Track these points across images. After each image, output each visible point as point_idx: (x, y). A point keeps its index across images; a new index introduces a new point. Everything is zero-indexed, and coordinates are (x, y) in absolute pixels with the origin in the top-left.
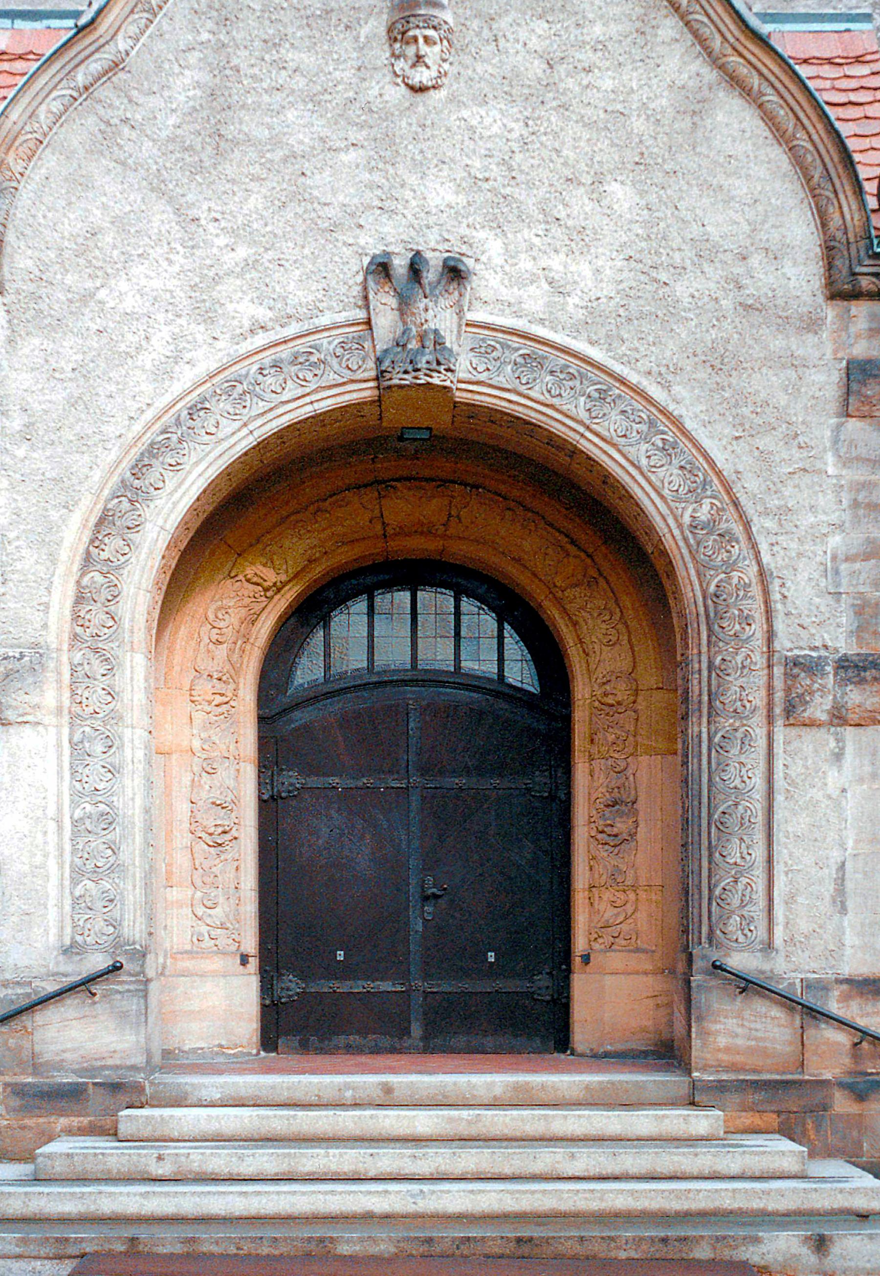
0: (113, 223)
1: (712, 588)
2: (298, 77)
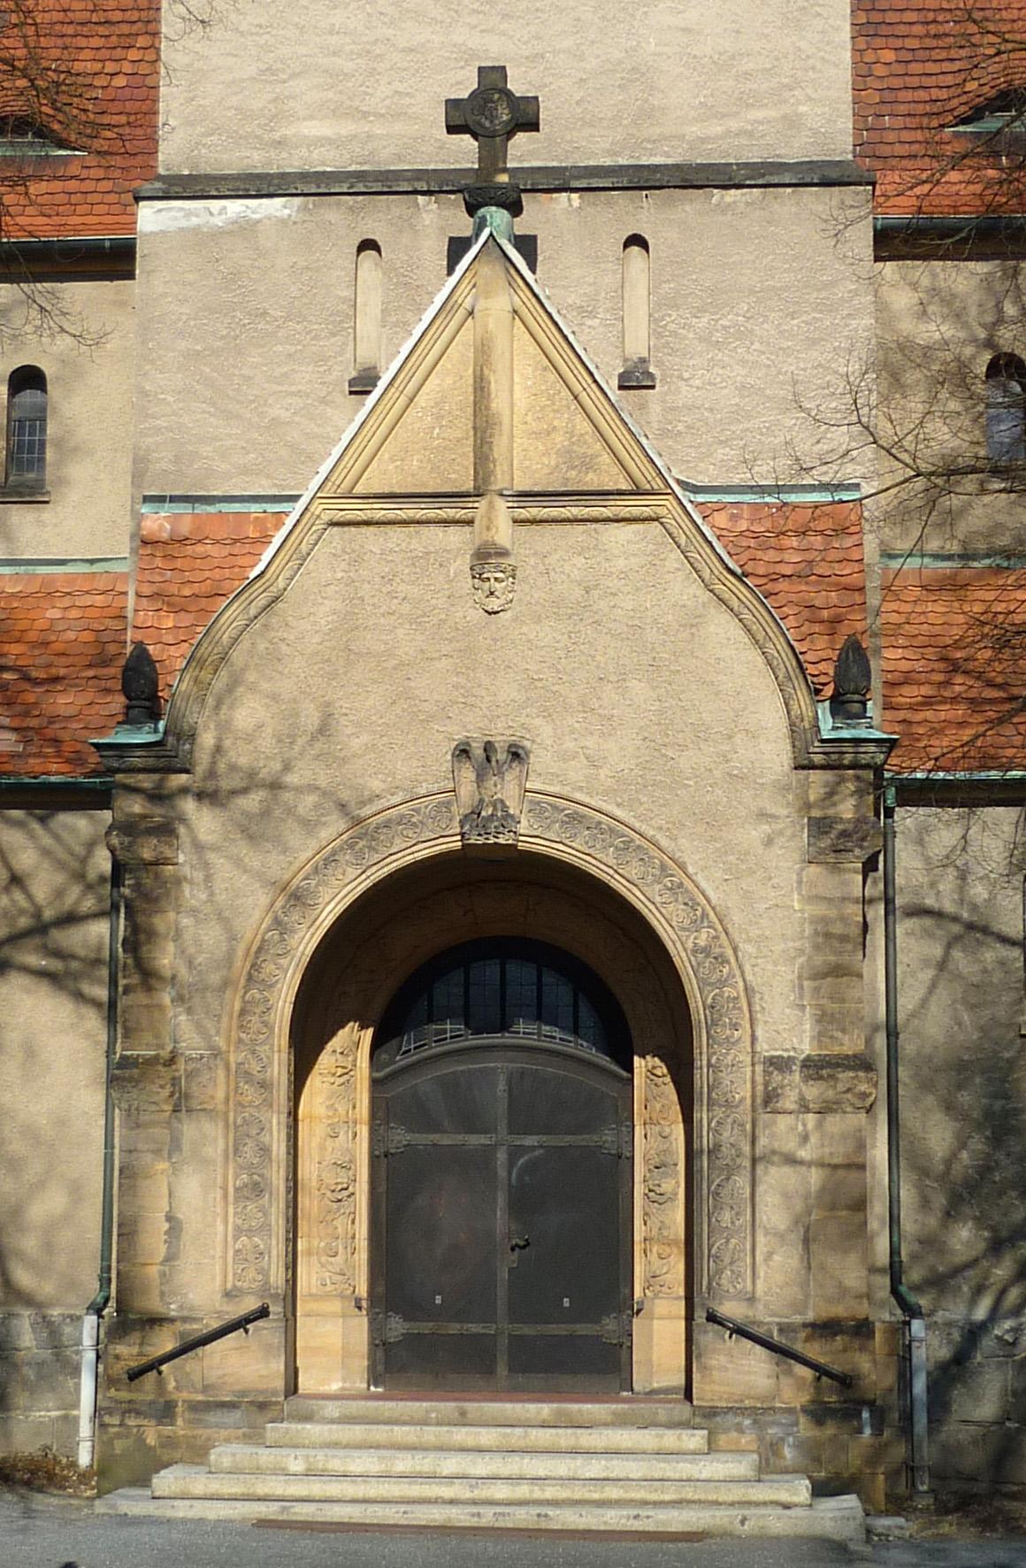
1: (709, 1001)
2: (405, 604)
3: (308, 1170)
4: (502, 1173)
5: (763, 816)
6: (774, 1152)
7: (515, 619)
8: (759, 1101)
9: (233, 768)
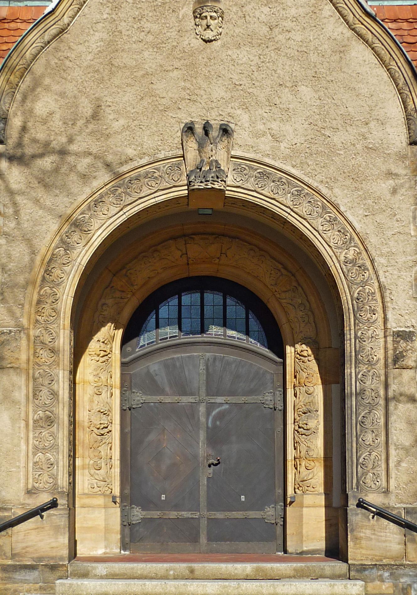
0: (60, 108)
1: (356, 295)
2: (149, 35)
3: (82, 415)
4: (203, 419)
5: (390, 174)
6: (401, 395)
7: (223, 46)
8: (390, 360)
9: (34, 141)
